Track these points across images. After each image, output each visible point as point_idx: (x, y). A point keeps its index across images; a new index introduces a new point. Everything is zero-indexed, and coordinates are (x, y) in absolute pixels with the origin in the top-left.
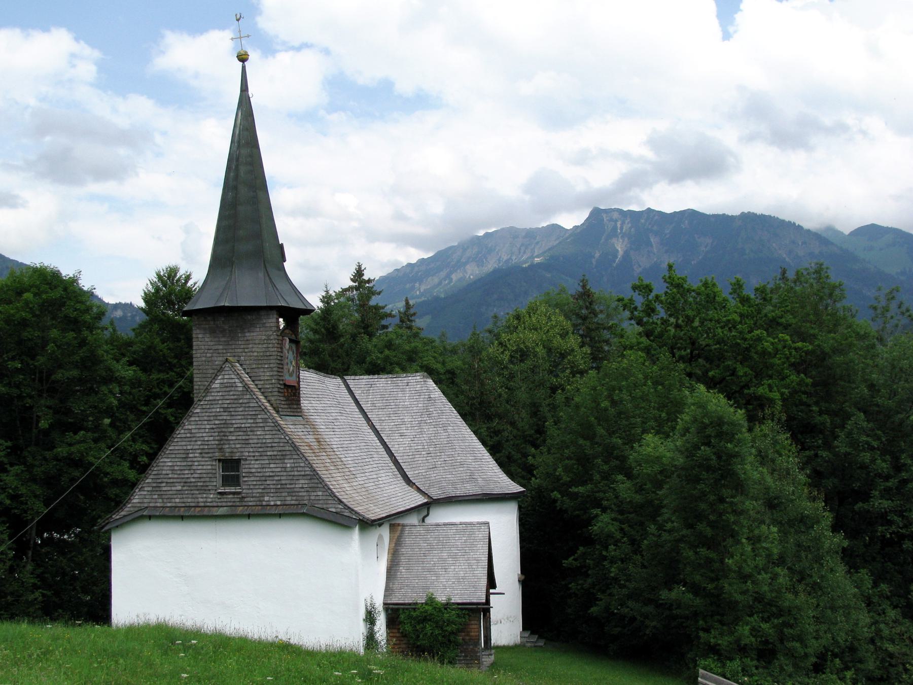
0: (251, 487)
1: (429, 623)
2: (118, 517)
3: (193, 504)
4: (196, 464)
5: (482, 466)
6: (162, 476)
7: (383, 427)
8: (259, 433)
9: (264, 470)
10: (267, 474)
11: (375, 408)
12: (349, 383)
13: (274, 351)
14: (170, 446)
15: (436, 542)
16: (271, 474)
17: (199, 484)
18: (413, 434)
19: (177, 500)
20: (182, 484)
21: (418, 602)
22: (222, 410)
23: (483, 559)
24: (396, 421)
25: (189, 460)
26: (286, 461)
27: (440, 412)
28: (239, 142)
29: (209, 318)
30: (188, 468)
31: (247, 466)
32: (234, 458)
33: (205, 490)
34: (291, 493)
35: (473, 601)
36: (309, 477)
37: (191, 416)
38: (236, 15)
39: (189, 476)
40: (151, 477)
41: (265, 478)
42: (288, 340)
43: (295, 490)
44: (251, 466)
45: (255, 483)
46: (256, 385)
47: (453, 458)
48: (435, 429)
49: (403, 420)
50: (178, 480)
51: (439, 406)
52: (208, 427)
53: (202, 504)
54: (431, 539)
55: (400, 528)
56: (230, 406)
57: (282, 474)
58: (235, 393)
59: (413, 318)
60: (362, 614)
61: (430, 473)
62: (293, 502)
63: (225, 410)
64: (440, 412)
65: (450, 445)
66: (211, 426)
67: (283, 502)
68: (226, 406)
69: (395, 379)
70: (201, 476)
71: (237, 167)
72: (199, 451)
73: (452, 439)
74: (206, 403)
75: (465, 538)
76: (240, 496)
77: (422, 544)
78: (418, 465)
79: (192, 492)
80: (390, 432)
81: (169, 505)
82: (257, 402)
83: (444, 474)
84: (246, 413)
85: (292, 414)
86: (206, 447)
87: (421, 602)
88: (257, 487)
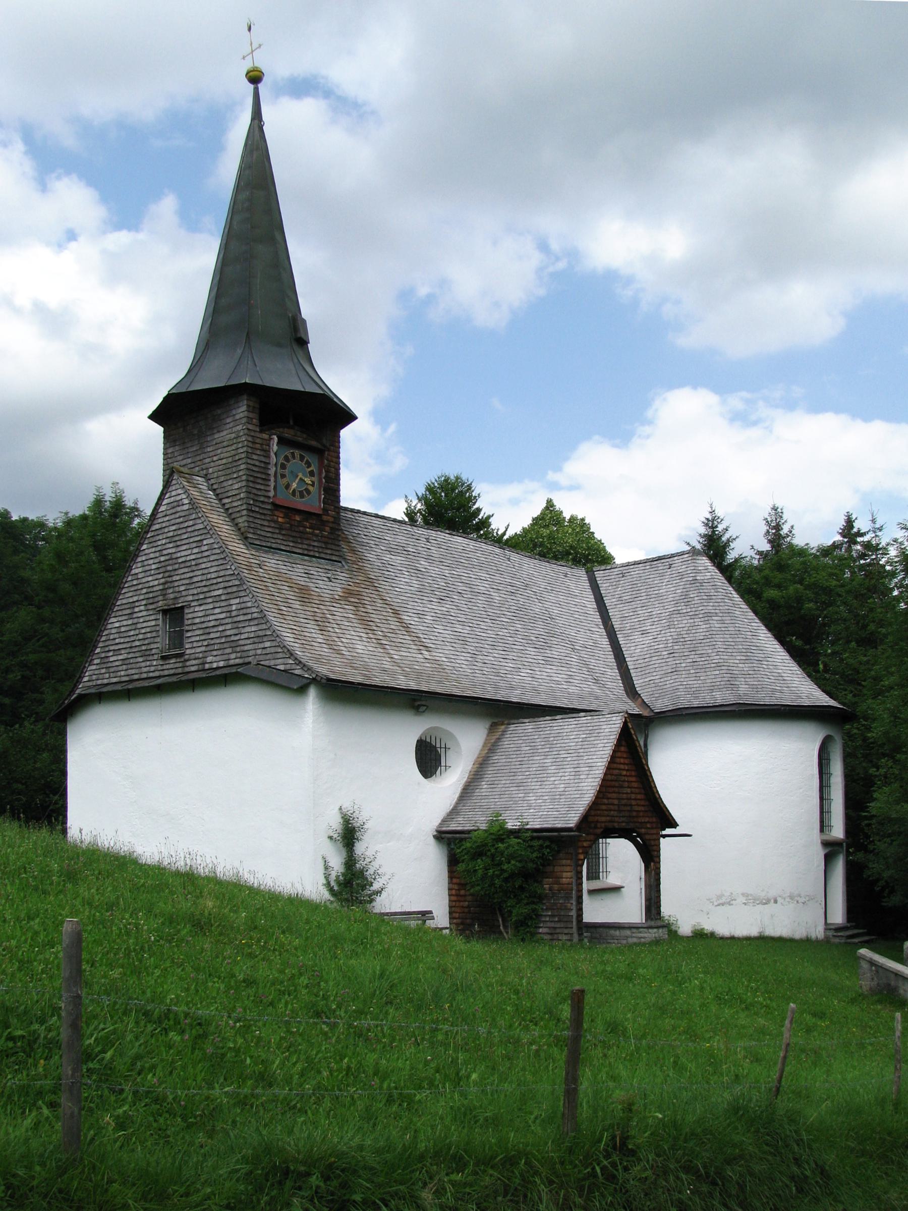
4: (141, 620)
14: (118, 600)
19: (123, 673)
21: (481, 828)
25: (135, 615)
30: (133, 627)
36: (256, 622)
47: (708, 658)
48: (692, 621)
55: (503, 727)
57: (227, 621)
72: (144, 602)
77: (522, 749)
78: (652, 670)
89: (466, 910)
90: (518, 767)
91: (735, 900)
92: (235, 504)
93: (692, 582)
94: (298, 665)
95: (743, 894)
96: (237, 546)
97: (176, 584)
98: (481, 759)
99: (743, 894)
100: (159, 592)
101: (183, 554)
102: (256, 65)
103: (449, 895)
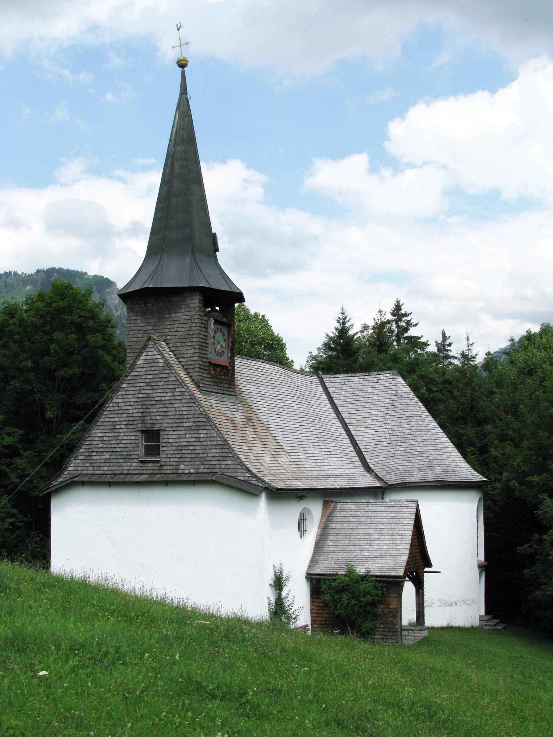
0: (169, 456)
1: (346, 593)
2: (56, 483)
3: (118, 472)
4: (122, 434)
5: (442, 456)
6: (93, 446)
7: (351, 420)
8: (176, 405)
9: (181, 440)
10: (183, 444)
11: (346, 403)
12: (325, 381)
13: (196, 329)
14: (100, 418)
15: (364, 518)
16: (187, 444)
17: (124, 453)
18: (378, 425)
19: (106, 468)
20: (110, 453)
21: (339, 573)
22: (145, 384)
23: (407, 534)
24: (364, 414)
25: (116, 431)
26: (200, 432)
27: (405, 406)
28: (175, 140)
29: (141, 302)
30: (115, 438)
31: (165, 437)
32: (154, 429)
33: (129, 459)
34: (204, 461)
35: (391, 574)
36: (220, 447)
37: (118, 391)
38: (177, 25)
39: (116, 446)
40: (84, 446)
41: (180, 449)
42: (213, 321)
43: (208, 459)
44: (169, 437)
45: (172, 452)
46: (180, 362)
47: (413, 448)
48: (399, 421)
49: (370, 414)
50: (107, 450)
51: (405, 401)
52: (133, 400)
53: (126, 472)
54: (361, 515)
55: (333, 504)
56: (152, 380)
57: (196, 443)
58: (157, 368)
59: (449, 348)
60: (270, 578)
61: (389, 461)
62: (205, 471)
63: (148, 384)
64: (405, 406)
65: (412, 436)
66: (136, 400)
67: (196, 470)
68: (148, 380)
69: (366, 377)
70: (126, 445)
71: (172, 163)
73: (415, 430)
74: (132, 378)
75: (393, 515)
76: (159, 465)
77: (351, 520)
78: (378, 454)
79: (118, 461)
80: (357, 424)
81: (98, 472)
82: (176, 377)
83: (402, 462)
84: (166, 387)
85: (220, 392)
86: (131, 419)
87: (341, 573)
88: (174, 456)
89: (323, 623)
90: (350, 532)
91: (434, 604)
92: (189, 363)
93: (396, 394)
94: (254, 478)
95: (439, 600)
96: (197, 394)
97: (153, 414)
98: (322, 525)
99: (439, 600)
100: (139, 418)
101: (158, 395)
102: (184, 55)
103: (311, 613)
